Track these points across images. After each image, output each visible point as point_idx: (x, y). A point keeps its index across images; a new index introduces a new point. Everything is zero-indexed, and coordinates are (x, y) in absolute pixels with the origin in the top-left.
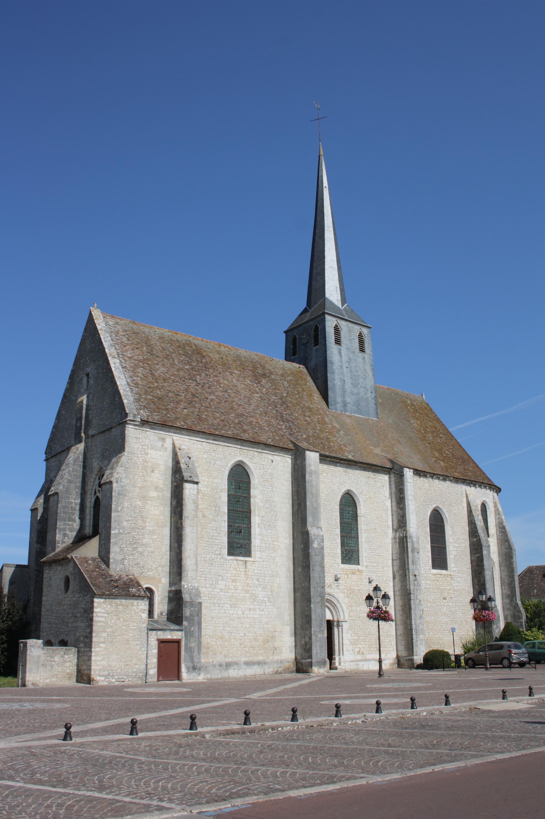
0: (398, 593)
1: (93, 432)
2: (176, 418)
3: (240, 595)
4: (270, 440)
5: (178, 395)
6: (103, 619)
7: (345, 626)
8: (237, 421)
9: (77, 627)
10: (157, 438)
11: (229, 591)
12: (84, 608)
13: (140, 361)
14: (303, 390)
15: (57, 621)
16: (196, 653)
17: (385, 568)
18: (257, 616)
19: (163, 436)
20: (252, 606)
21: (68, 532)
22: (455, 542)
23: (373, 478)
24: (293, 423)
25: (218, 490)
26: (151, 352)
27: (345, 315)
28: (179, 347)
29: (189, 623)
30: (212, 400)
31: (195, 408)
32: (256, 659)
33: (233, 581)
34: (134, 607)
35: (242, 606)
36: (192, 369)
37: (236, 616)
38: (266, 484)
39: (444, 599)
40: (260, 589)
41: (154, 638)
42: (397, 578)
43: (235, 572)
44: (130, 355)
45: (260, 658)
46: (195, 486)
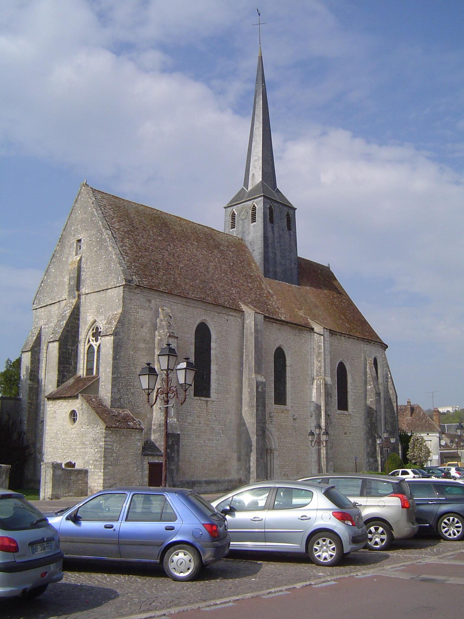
1: (87, 290)
2: (159, 284)
3: (203, 428)
4: (226, 303)
5: (157, 263)
6: (110, 447)
7: (276, 453)
8: (201, 286)
9: (86, 452)
10: (145, 300)
11: (195, 424)
12: (93, 438)
13: (125, 232)
14: (244, 261)
15: (63, 447)
16: (175, 474)
17: (305, 409)
18: (214, 445)
19: (150, 298)
20: (211, 437)
21: (66, 374)
22: (354, 389)
23: (298, 336)
24: (240, 288)
25: (189, 344)
26: (132, 224)
27: (277, 198)
28: (151, 220)
29: (171, 450)
30: (182, 268)
31: (171, 274)
32: (212, 479)
33: (198, 417)
34: (133, 438)
35: (203, 437)
36: (164, 240)
37: (199, 444)
38: (223, 339)
39: (346, 434)
40: (217, 423)
41: (147, 461)
43: (199, 409)
44: (117, 227)
45: (216, 478)
46: (176, 340)
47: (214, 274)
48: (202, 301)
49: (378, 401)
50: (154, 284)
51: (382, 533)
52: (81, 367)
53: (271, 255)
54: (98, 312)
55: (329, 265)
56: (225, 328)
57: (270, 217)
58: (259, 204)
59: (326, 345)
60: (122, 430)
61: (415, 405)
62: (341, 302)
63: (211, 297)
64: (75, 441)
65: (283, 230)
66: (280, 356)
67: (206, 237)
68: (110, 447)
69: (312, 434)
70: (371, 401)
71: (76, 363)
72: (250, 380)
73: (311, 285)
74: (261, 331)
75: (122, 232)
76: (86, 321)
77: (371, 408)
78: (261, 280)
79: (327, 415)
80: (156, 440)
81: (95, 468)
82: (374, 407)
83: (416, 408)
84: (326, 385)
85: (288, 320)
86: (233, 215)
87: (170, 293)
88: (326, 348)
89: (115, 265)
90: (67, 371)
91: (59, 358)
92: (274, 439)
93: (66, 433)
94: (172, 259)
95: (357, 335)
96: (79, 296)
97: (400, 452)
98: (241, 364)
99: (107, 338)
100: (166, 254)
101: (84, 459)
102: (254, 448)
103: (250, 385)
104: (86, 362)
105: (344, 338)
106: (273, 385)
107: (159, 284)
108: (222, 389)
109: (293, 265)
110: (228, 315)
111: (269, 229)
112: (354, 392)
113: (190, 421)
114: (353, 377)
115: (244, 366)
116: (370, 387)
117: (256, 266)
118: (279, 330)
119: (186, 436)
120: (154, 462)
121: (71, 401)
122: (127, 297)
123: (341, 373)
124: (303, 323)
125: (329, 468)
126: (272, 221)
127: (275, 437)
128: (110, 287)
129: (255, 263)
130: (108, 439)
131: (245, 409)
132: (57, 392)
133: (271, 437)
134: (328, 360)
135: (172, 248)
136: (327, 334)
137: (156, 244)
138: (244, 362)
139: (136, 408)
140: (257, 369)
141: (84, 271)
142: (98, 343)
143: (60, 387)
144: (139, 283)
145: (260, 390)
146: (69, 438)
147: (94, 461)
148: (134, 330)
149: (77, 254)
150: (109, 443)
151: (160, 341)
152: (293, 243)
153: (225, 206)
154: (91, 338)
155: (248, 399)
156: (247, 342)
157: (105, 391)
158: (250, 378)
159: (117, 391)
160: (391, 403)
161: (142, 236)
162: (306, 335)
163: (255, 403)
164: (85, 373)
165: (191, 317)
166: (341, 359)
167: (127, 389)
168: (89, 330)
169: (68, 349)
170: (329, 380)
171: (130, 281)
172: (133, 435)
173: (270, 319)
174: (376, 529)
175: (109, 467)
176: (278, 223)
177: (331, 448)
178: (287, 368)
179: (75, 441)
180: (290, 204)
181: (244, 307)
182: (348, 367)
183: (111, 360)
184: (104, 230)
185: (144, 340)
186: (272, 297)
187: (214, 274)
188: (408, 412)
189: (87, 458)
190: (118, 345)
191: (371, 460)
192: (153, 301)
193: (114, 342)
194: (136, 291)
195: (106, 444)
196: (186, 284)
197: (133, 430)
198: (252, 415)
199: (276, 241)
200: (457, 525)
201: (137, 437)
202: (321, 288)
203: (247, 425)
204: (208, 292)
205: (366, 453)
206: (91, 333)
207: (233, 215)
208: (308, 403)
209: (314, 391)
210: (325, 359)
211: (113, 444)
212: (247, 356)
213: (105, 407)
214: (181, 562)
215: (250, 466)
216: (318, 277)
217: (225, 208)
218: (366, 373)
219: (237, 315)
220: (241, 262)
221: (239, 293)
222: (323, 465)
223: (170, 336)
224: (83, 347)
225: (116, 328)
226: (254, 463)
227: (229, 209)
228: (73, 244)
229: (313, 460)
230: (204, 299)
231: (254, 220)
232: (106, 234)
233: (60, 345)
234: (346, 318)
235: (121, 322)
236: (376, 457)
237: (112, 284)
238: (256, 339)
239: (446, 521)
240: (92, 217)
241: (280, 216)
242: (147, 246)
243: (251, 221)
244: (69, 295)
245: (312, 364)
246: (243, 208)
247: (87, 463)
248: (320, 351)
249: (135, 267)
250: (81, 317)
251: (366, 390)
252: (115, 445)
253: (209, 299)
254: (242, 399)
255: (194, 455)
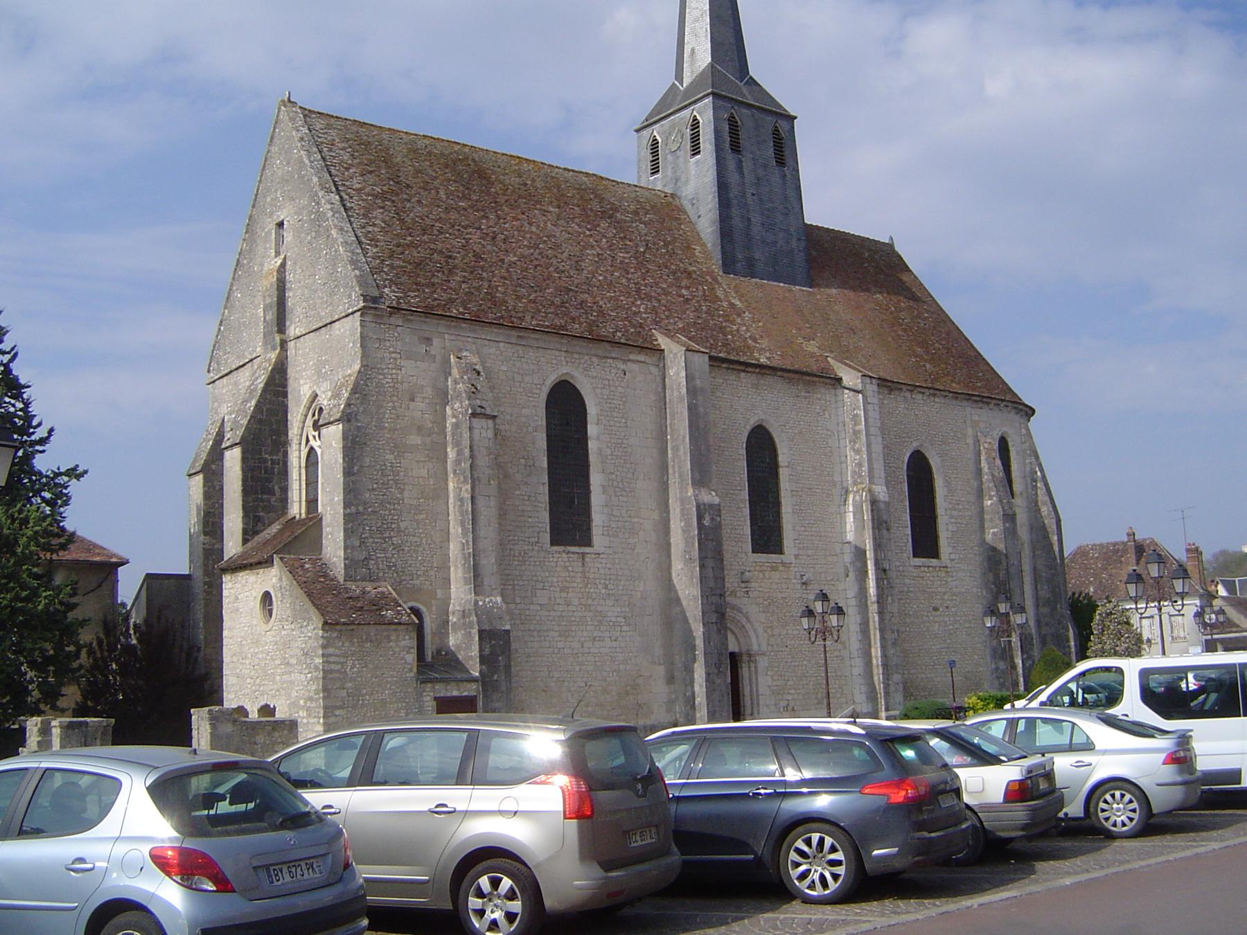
4: (619, 334)
5: (450, 257)
6: (338, 667)
7: (762, 662)
8: (557, 300)
9: (292, 682)
11: (556, 607)
13: (376, 196)
14: (675, 240)
17: (830, 559)
23: (805, 398)
24: (659, 301)
25: (530, 429)
28: (447, 166)
30: (512, 264)
39: (936, 609)
44: (358, 186)
46: (490, 422)
47: (593, 273)
48: (557, 332)
49: (1011, 532)
50: (435, 303)
51: (511, 896)
52: (296, 498)
53: (737, 222)
54: (319, 373)
55: (891, 239)
56: (620, 389)
57: (731, 140)
58: (704, 112)
59: (871, 414)
60: (366, 628)
61: (1144, 540)
62: (918, 317)
63: (581, 323)
65: (765, 166)
66: (761, 446)
67: (589, 199)
68: (338, 667)
69: (810, 613)
70: (993, 532)
71: (285, 490)
72: (683, 501)
73: (844, 285)
74: (702, 390)
75: (368, 195)
76: (300, 396)
77: (994, 549)
78: (715, 279)
79: (881, 571)
80: (457, 646)
81: (309, 715)
82: (1001, 547)
83: (1149, 546)
84: (874, 502)
85: (777, 362)
86: (655, 144)
87: (476, 320)
88: (871, 420)
89: (344, 267)
90: (264, 508)
91: (244, 481)
92: (755, 631)
93: (256, 643)
94: (489, 247)
95: (955, 387)
96: (283, 344)
97: (1072, 644)
98: (664, 468)
99: (332, 428)
100: (476, 237)
101: (289, 696)
102: (700, 652)
103: (684, 512)
104: (304, 486)
105: (920, 396)
106: (747, 512)
107: (451, 301)
108: (620, 524)
109: (794, 243)
110: (625, 361)
111: (731, 165)
112: (952, 517)
113: (544, 601)
114: (947, 483)
115: (670, 471)
116: (989, 502)
117: (704, 252)
118: (755, 386)
119: (535, 633)
120: (449, 694)
121: (261, 571)
122: (371, 334)
123: (919, 476)
124: (814, 368)
125: (892, 689)
126: (736, 147)
127: (756, 625)
128: (336, 317)
129: (704, 245)
130: (331, 650)
131: (677, 566)
132: (243, 556)
133: (748, 626)
134: (877, 448)
135: (491, 223)
136: (872, 388)
137: (453, 216)
138: (671, 464)
139: (408, 578)
140: (697, 476)
141: (290, 289)
143: (249, 545)
144: (399, 303)
145: (706, 522)
146: (262, 652)
148: (394, 408)
150: (332, 659)
151: (456, 426)
152: (791, 193)
153: (638, 127)
154: (312, 433)
155: (682, 545)
156: (673, 418)
157: (333, 547)
158: (683, 496)
159: (357, 543)
160: (1046, 537)
161: (419, 201)
162: (823, 394)
163: (696, 554)
164: (303, 511)
165: (529, 373)
166: (915, 444)
167: (384, 539)
168: (306, 416)
169: (266, 460)
170: (881, 491)
171: (375, 300)
172: (393, 638)
173: (728, 363)
174: (495, 883)
175: (337, 712)
176: (751, 152)
177: (894, 644)
178: (781, 471)
180: (780, 106)
181: (663, 341)
182: (934, 462)
183: (340, 476)
184: (321, 194)
185: (420, 429)
186: (739, 315)
187: (593, 273)
188: (1131, 556)
189: (294, 694)
190: (354, 442)
191: (1002, 665)
192: (436, 341)
193: (345, 437)
194: (393, 320)
195: (328, 662)
196: (519, 298)
197: (393, 627)
198: (692, 579)
199: (750, 190)
200: (833, 856)
201: (403, 643)
202: (868, 290)
203: (684, 603)
204: (574, 313)
205: (988, 652)
206: (309, 422)
207: (655, 144)
208: (838, 548)
209: (850, 518)
210: (869, 446)
211: (342, 660)
212: (676, 449)
213: (332, 580)
214: (816, 869)
215: (693, 693)
216: (866, 267)
217: (638, 131)
218: (979, 472)
219: (648, 360)
220: (666, 245)
221: (654, 310)
222: (876, 683)
223: (474, 415)
224: (296, 454)
225: (348, 405)
226: (701, 686)
227: (646, 133)
228: (269, 233)
229: (856, 671)
230: (563, 327)
231: (696, 150)
232: (328, 203)
233: (243, 453)
234: (927, 353)
235: (361, 389)
236: (1012, 658)
237: (341, 310)
238: (692, 409)
239: (800, 844)
240: (300, 169)
241: (754, 134)
242: (428, 222)
243: (689, 153)
244: (265, 344)
245: (843, 459)
246: (673, 127)
248: (857, 428)
249: (392, 267)
250: (290, 389)
251: (981, 511)
252: (350, 663)
253: (576, 328)
254: (669, 544)
255: (556, 674)
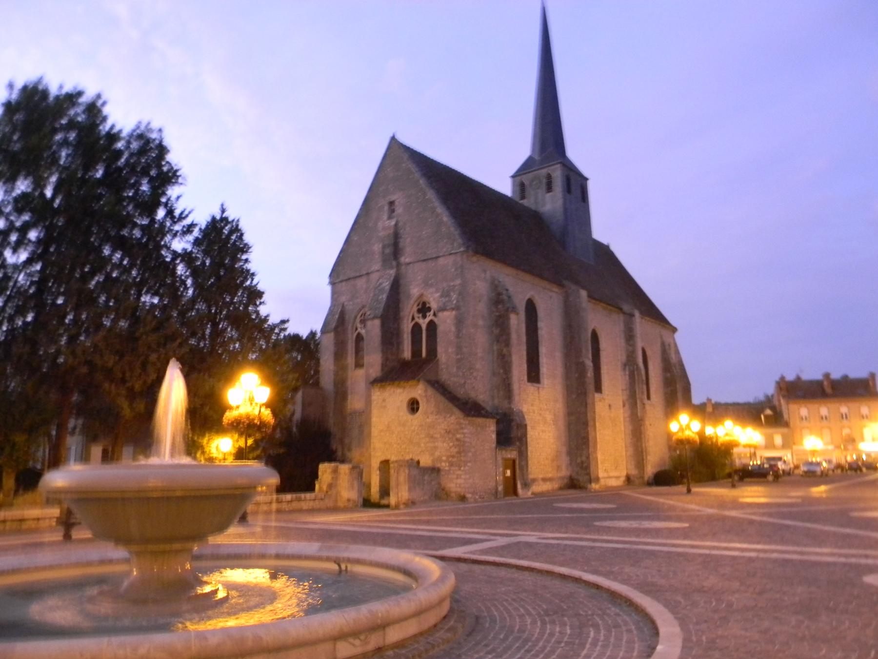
0: (628, 419)
42: (627, 406)
55: (268, 316)
57: (568, 188)
64: (418, 434)
142: (427, 320)
147: (448, 457)
149: (390, 218)
179: (418, 434)
189: (437, 454)
192: (488, 272)
227: (518, 178)
231: (549, 188)
247: (439, 459)
